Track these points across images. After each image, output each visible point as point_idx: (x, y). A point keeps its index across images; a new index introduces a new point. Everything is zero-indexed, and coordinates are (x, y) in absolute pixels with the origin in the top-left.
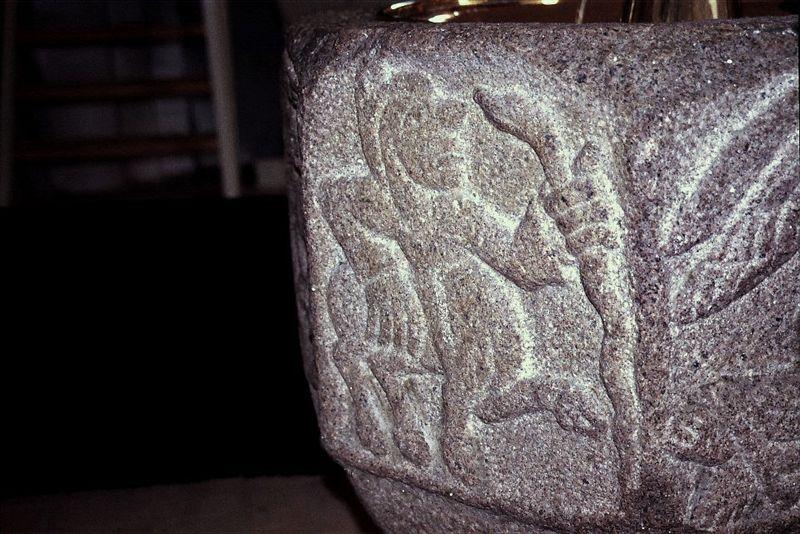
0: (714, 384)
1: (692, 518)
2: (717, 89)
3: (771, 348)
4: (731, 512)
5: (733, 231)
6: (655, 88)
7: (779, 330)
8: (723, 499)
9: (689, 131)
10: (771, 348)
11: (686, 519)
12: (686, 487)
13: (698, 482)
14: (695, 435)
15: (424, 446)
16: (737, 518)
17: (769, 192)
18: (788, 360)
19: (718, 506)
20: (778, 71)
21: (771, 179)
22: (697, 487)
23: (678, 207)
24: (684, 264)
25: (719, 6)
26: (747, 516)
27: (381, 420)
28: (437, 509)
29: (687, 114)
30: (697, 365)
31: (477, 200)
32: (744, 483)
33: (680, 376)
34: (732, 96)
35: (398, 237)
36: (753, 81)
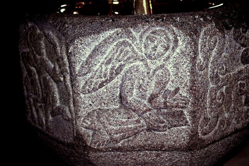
0: (96, 110)
1: (90, 144)
2: (90, 34)
3: (112, 102)
4: (101, 143)
5: (97, 71)
6: (74, 34)
7: (114, 97)
8: (98, 140)
9: (83, 45)
10: (112, 102)
11: (89, 144)
12: (89, 136)
13: (92, 135)
14: (89, 123)
15: (43, 123)
16: (103, 145)
17: (105, 61)
18: (117, 105)
19: (97, 142)
20: (106, 31)
21: (106, 58)
22: (92, 137)
23: (81, 64)
24: (85, 79)
25: (147, 9)
26: (106, 145)
27: (36, 115)
28: (142, 156)
29: (81, 40)
30: (91, 105)
31: (47, 59)
32: (104, 136)
33: (86, 107)
34: (94, 37)
35: (35, 67)
36: (99, 33)
